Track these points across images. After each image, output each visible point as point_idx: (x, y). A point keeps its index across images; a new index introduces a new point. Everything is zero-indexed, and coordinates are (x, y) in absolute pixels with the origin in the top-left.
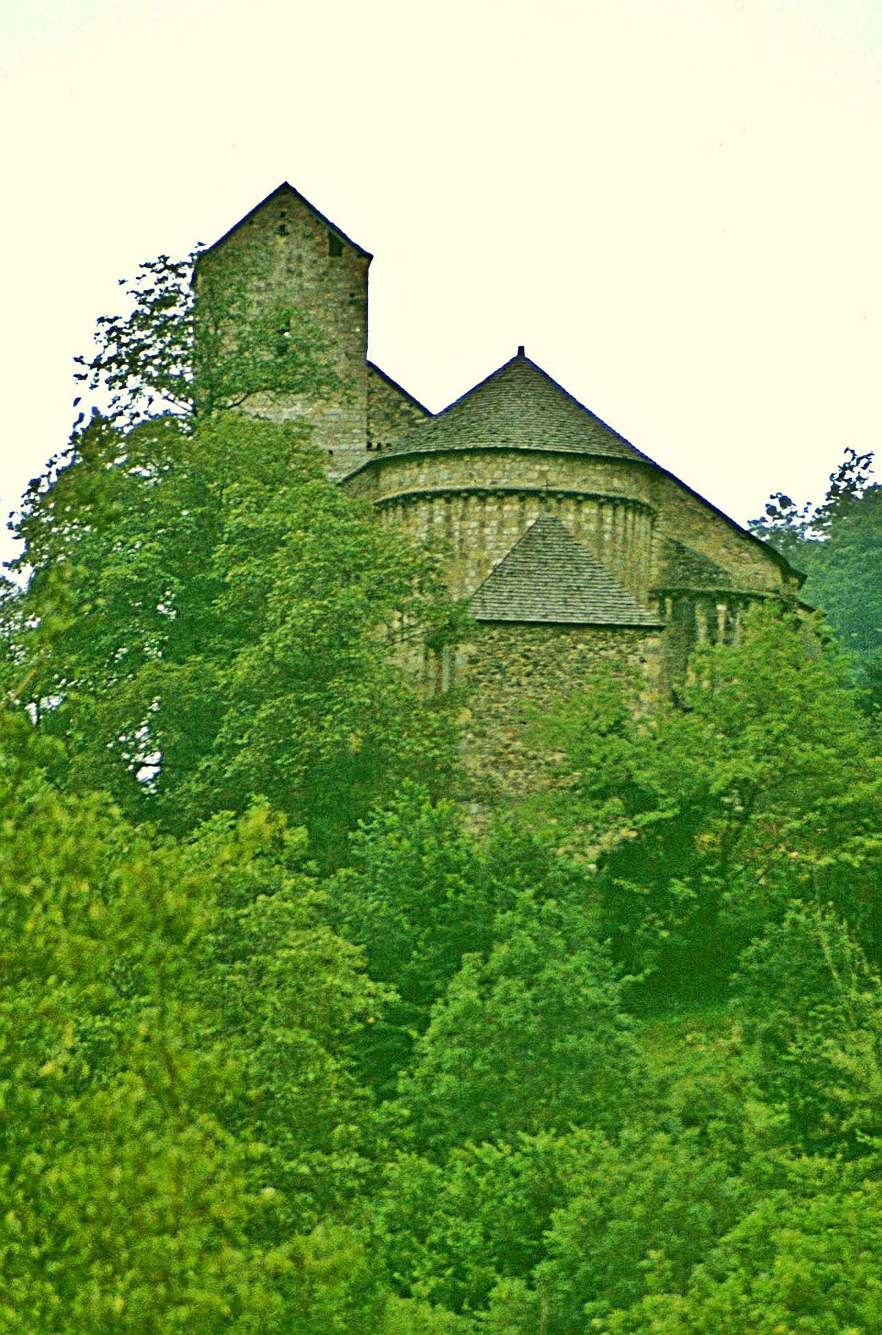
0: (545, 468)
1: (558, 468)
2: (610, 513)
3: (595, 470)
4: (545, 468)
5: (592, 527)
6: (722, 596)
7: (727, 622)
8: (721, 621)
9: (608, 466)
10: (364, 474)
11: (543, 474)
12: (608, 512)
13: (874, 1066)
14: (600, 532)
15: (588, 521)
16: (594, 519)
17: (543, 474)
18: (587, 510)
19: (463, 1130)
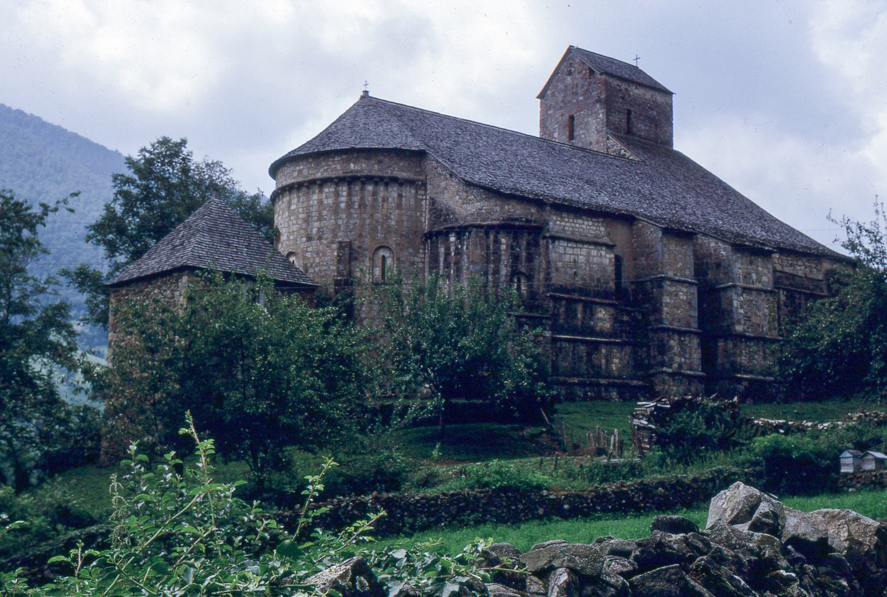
0: (302, 167)
1: (309, 166)
2: (345, 188)
3: (333, 161)
4: (302, 167)
5: (330, 201)
6: (450, 230)
7: (457, 248)
8: (452, 248)
9: (344, 157)
10: (763, 296)
11: (300, 171)
12: (344, 190)
13: (458, 467)
14: (337, 204)
15: (327, 198)
16: (332, 195)
17: (300, 171)
18: (327, 190)
19: (76, 198)
